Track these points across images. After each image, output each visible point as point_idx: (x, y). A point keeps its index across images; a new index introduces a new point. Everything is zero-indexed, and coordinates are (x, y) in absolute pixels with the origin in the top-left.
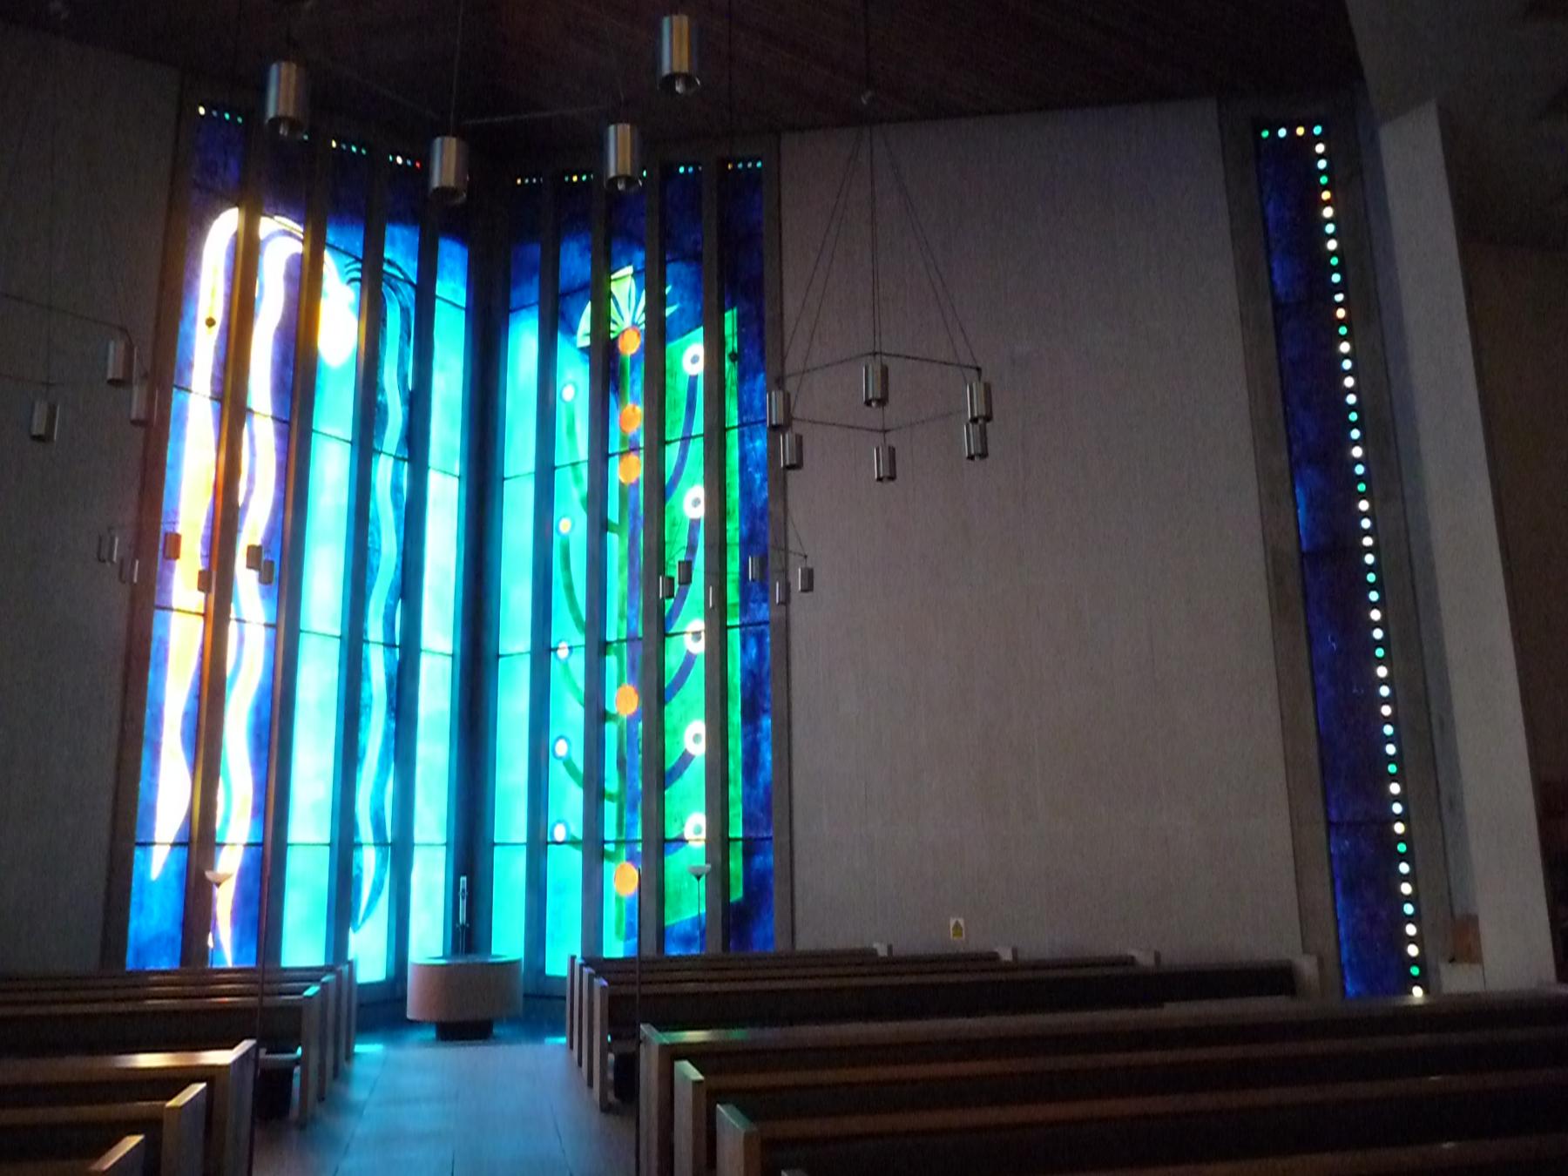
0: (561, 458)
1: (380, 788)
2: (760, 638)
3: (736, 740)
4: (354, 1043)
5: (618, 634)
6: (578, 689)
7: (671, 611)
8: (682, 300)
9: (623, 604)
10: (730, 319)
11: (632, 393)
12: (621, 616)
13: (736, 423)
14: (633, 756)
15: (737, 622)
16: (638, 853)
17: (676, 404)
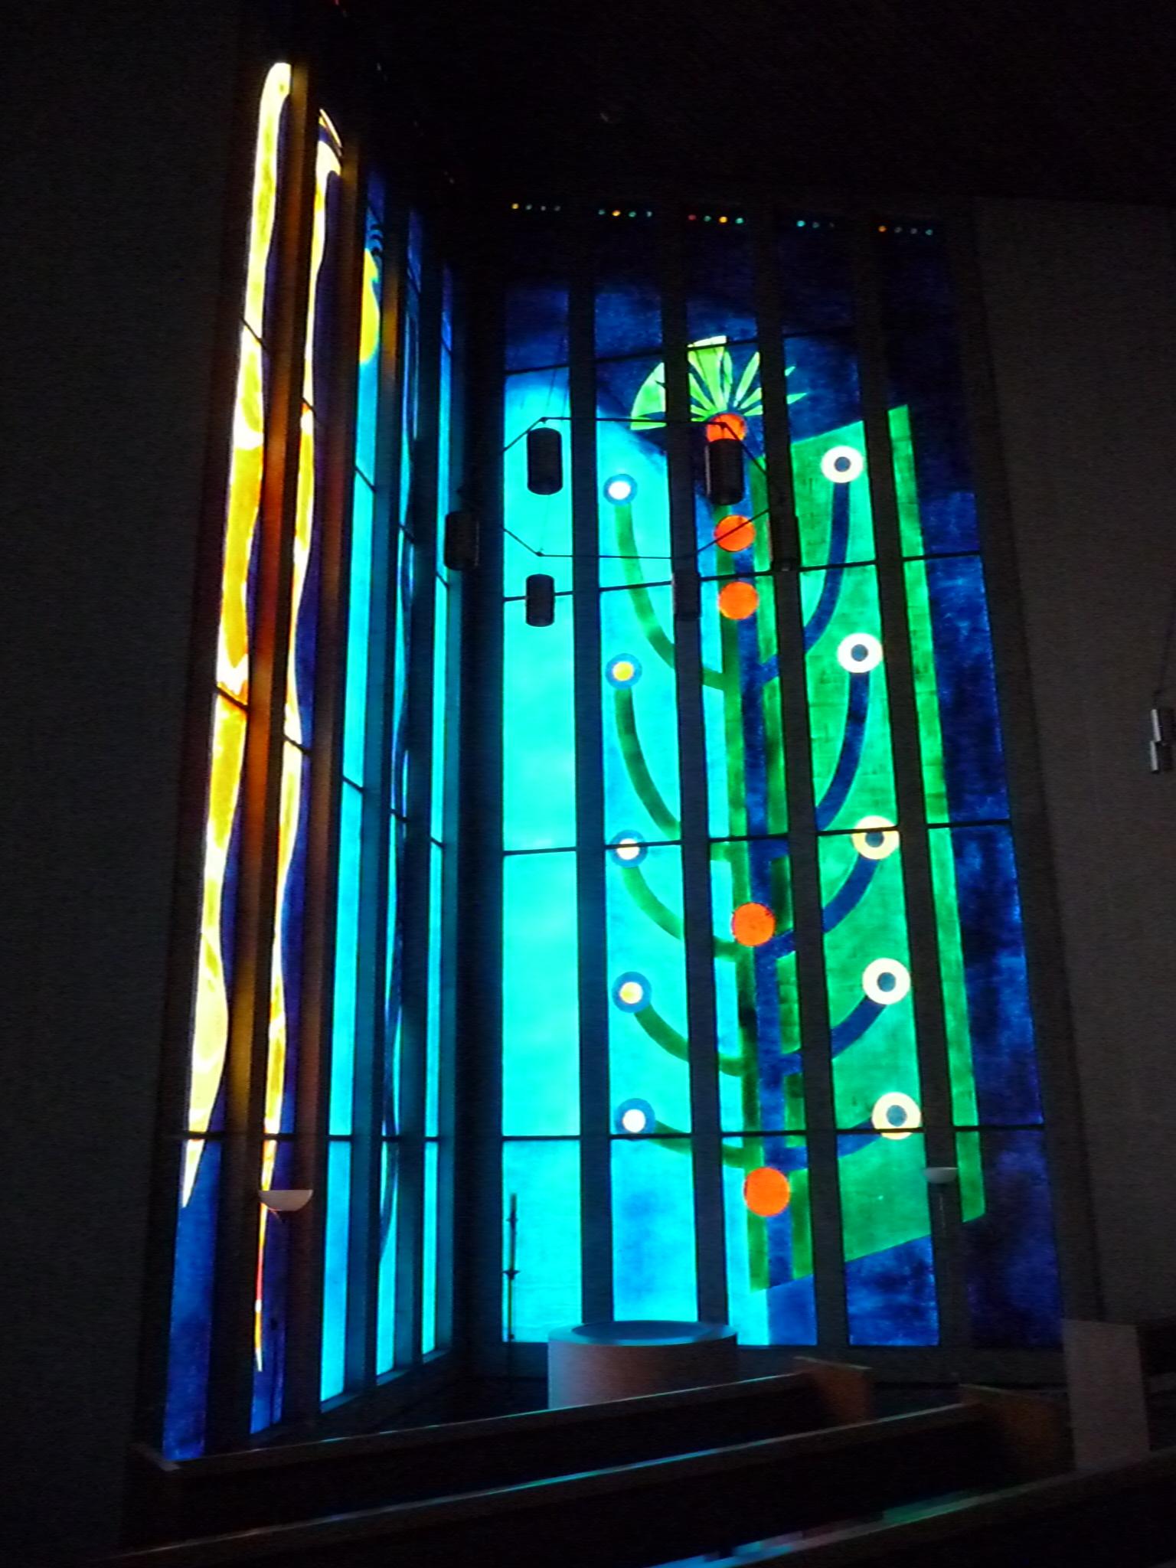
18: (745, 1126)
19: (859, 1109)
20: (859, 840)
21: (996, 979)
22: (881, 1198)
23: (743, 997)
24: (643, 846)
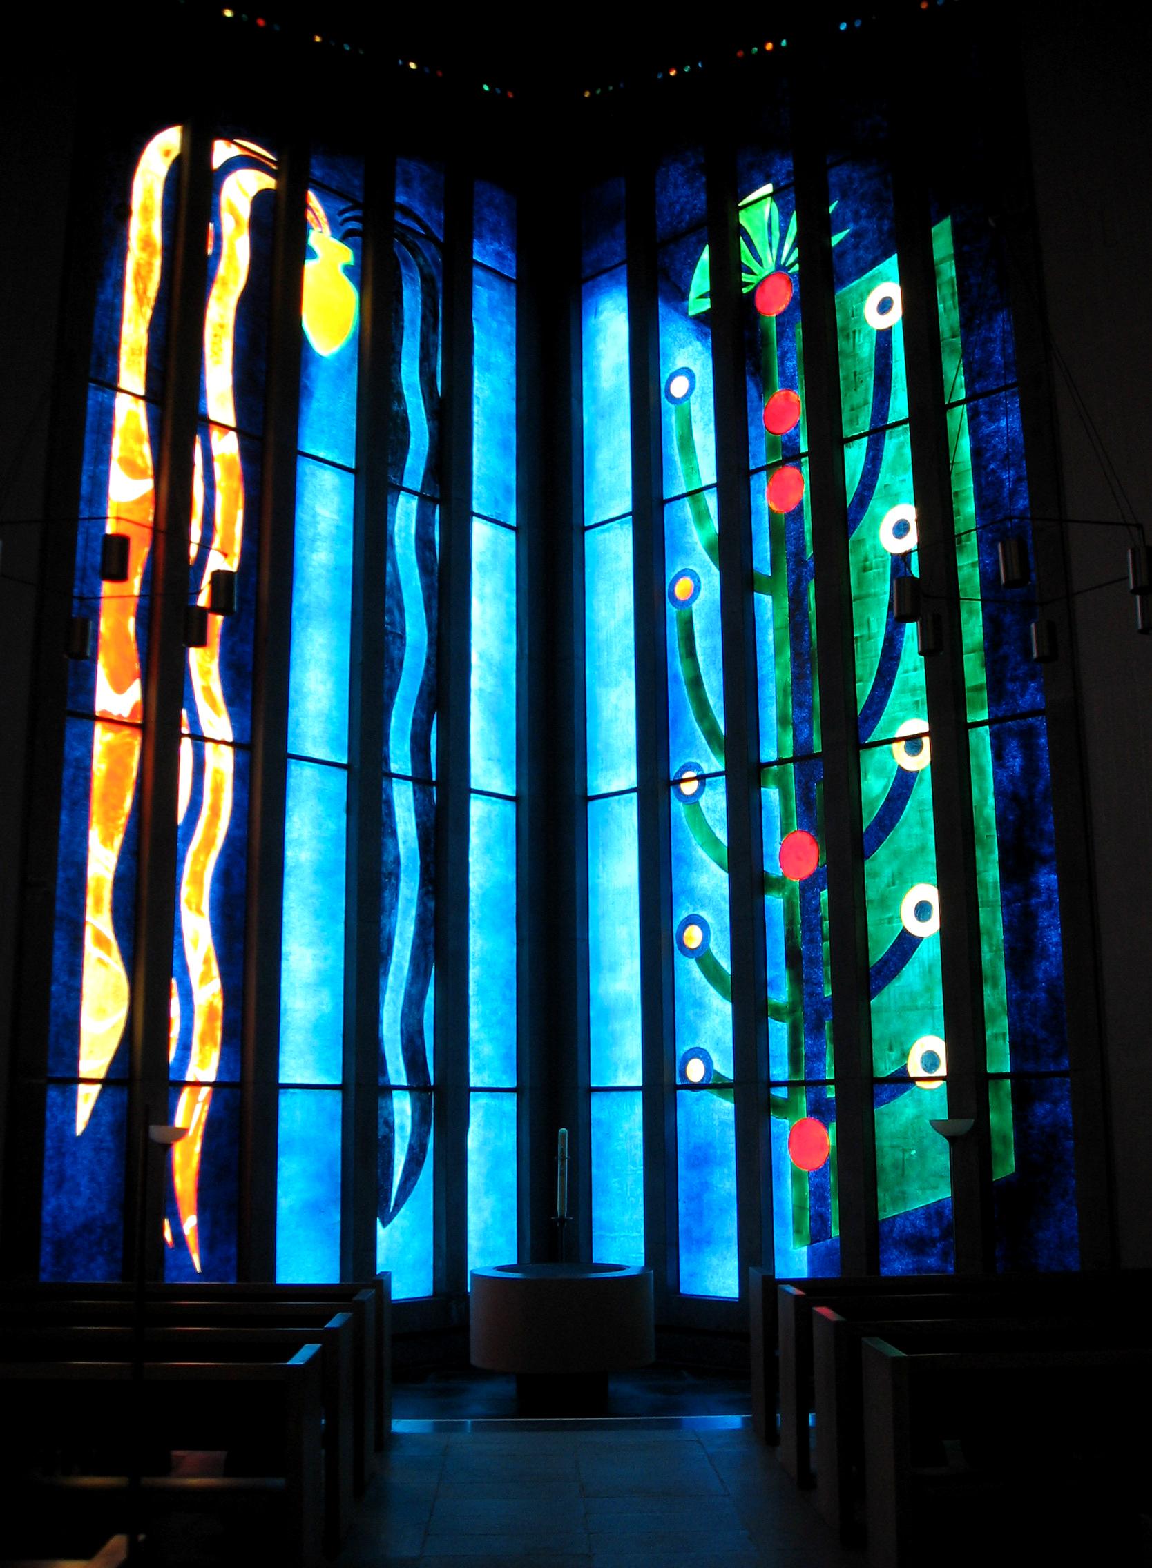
0: (677, 484)
1: (413, 1003)
2: (1027, 738)
3: (994, 913)
4: (390, 1418)
5: (779, 751)
6: (717, 841)
7: (867, 706)
8: (857, 217)
9: (785, 704)
10: (942, 239)
11: (782, 373)
12: (782, 721)
13: (962, 394)
14: (813, 942)
15: (984, 715)
16: (830, 1100)
17: (856, 380)
18: (789, 1076)
19: (894, 1055)
20: (899, 748)
21: (1034, 901)
22: (913, 1152)
23: (790, 935)
24: (702, 778)
